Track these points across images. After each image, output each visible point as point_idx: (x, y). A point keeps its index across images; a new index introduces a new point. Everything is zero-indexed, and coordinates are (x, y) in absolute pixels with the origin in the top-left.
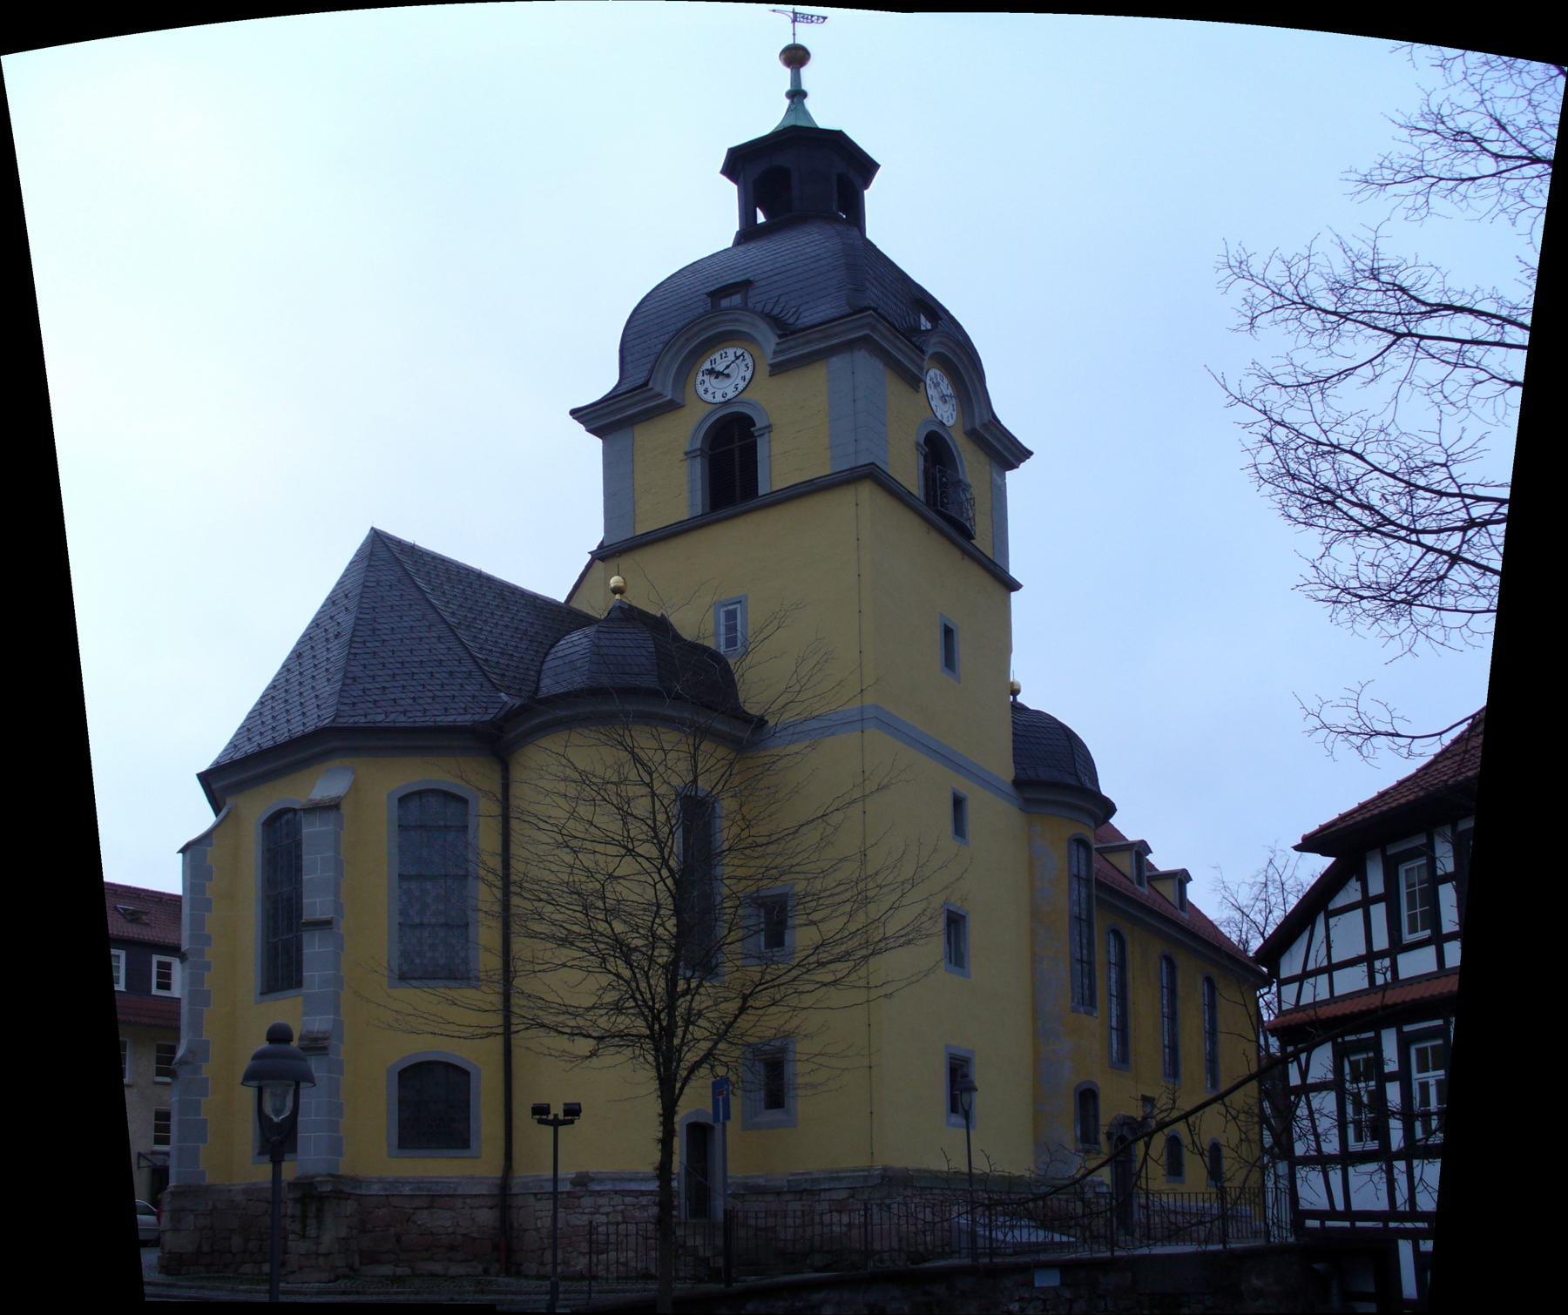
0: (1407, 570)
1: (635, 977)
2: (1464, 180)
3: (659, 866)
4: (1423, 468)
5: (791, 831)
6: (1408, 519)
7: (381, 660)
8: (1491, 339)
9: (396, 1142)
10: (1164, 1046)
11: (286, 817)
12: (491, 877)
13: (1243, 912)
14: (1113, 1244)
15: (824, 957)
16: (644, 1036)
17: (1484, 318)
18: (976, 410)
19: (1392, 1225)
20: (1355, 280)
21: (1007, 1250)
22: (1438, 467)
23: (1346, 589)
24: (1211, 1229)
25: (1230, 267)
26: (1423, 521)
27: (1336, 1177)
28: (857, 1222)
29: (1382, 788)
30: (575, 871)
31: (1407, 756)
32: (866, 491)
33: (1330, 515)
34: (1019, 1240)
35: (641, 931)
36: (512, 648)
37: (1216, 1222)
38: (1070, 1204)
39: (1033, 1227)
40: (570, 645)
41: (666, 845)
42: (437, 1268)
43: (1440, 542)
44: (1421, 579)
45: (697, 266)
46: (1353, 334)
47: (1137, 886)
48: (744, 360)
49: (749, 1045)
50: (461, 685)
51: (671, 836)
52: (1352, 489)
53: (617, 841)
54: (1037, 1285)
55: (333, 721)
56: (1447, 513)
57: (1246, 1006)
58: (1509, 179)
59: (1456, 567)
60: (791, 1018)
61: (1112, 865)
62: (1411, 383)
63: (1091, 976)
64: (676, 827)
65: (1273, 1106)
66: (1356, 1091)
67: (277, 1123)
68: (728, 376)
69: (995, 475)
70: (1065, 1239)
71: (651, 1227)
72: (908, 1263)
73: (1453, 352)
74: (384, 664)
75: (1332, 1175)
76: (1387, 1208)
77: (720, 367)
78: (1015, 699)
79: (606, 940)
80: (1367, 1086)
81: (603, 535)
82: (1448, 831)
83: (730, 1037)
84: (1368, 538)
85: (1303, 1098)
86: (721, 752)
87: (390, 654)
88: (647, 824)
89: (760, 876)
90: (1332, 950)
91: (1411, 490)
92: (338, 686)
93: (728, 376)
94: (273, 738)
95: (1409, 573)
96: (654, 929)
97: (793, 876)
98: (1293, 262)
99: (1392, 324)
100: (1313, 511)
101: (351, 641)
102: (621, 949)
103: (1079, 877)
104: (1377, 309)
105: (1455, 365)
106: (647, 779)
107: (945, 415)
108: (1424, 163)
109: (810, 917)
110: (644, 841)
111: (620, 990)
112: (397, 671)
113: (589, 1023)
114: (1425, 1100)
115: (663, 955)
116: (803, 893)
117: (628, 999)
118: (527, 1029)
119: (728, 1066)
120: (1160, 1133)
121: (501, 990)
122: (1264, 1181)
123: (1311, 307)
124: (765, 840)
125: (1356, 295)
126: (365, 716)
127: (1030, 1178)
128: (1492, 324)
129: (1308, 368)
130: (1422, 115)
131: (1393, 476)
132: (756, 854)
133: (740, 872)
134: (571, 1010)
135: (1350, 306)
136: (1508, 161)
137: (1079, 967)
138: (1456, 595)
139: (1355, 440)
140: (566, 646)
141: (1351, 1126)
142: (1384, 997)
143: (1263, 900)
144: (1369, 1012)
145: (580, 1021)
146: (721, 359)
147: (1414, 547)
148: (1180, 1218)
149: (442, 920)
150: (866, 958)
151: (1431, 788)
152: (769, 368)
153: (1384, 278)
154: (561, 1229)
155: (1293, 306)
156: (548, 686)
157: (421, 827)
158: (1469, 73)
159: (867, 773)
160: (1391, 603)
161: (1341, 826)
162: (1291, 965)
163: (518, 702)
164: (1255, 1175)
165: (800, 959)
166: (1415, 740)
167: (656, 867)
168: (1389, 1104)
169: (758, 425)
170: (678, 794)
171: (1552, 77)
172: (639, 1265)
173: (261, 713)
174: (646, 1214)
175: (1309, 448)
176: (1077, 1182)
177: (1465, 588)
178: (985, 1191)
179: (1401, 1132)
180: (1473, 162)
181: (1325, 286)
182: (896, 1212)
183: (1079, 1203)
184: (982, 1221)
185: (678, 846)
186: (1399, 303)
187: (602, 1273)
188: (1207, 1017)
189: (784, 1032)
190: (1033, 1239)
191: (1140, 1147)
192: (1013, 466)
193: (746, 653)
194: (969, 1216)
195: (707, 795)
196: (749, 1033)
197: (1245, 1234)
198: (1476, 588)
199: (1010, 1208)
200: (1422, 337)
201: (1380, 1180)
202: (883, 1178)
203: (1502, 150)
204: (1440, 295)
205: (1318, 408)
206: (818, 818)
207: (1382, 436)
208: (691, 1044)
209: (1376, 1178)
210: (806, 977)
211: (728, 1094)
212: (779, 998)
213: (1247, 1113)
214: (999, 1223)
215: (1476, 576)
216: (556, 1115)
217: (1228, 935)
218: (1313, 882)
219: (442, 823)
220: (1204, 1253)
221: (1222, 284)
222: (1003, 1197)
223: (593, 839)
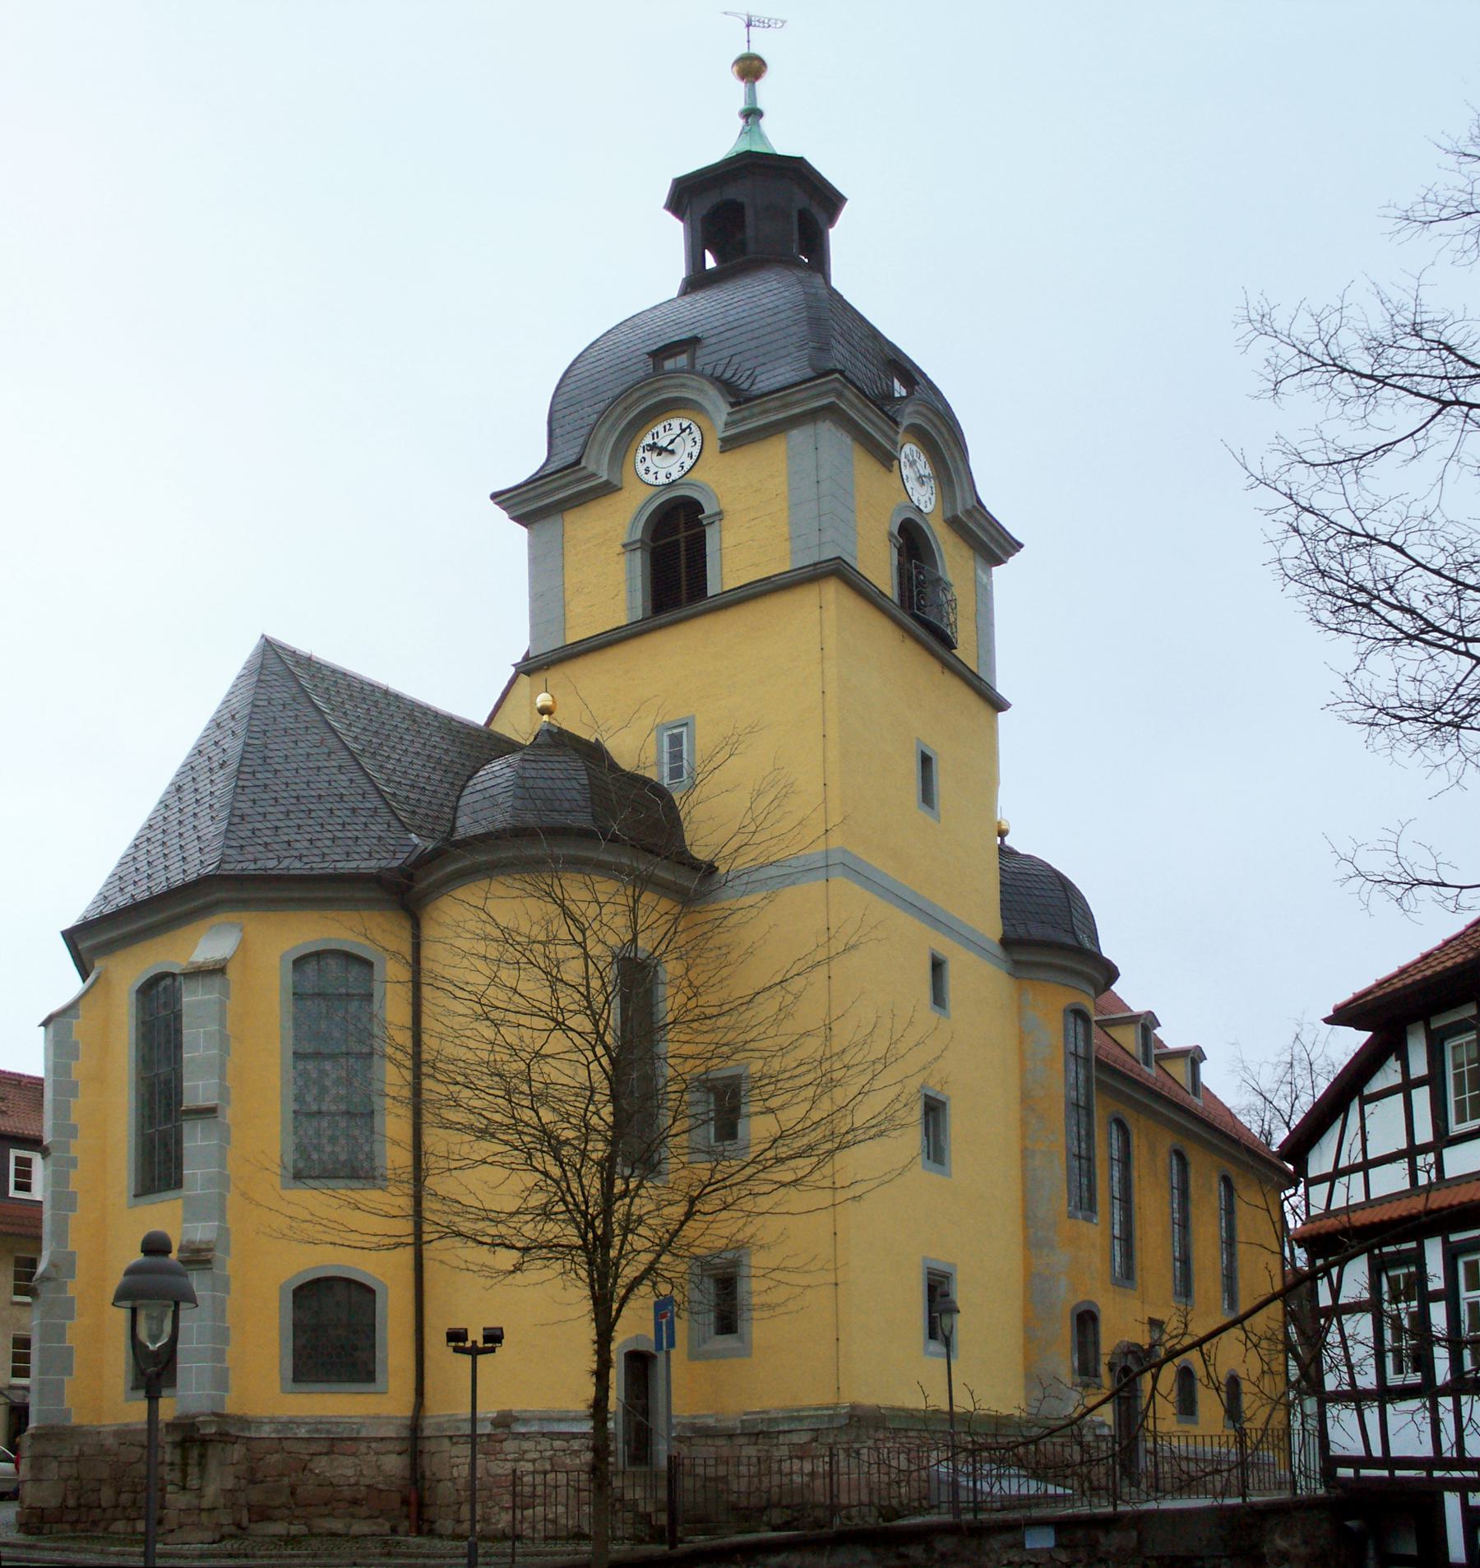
0: (1454, 686)
1: (566, 1176)
7: (274, 795)
9: (290, 1373)
11: (163, 984)
12: (399, 1056)
14: (1115, 1497)
15: (783, 1151)
16: (575, 1247)
18: (958, 494)
19: (1437, 1474)
24: (1228, 1480)
26: (1472, 627)
27: (1372, 1416)
28: (821, 1470)
29: (1426, 949)
30: (497, 1048)
32: (832, 592)
35: (572, 1120)
37: (1235, 1471)
39: (1024, 1476)
40: (491, 776)
41: (600, 1017)
42: (338, 1526)
44: (1470, 697)
46: (1392, 402)
47: (1143, 1066)
48: (690, 433)
49: (696, 1258)
50: (365, 824)
52: (1391, 589)
55: (218, 867)
57: (1268, 1211)
60: (745, 1225)
63: (1091, 1175)
65: (1301, 1332)
67: (153, 1352)
68: (672, 452)
69: (979, 572)
70: (1060, 1490)
71: (584, 1477)
72: (880, 1520)
74: (276, 799)
75: (1367, 1413)
79: (533, 1131)
80: (1409, 1307)
81: (528, 643)
85: (1335, 1321)
86: (665, 905)
87: (284, 787)
89: (709, 1055)
92: (223, 826)
93: (672, 452)
94: (149, 888)
95: (1456, 690)
98: (1323, 316)
101: (239, 772)
102: (549, 1142)
103: (1076, 1055)
104: (1420, 372)
106: (579, 938)
107: (922, 500)
109: (768, 1104)
110: (576, 1012)
112: (292, 808)
115: (598, 1149)
118: (440, 1238)
119: (672, 1283)
121: (411, 1192)
122: (1289, 1420)
123: (1344, 370)
124: (715, 1011)
126: (255, 861)
129: (1341, 443)
131: (1438, 573)
132: (705, 1028)
133: (686, 1050)
135: (1388, 367)
137: (1077, 1164)
140: (487, 777)
141: (1390, 1354)
144: (1411, 1218)
145: (503, 1229)
146: (664, 432)
147: (1462, 658)
148: (1192, 1466)
149: (343, 1107)
150: (831, 1153)
152: (719, 443)
153: (1427, 334)
154: (481, 1479)
155: (1323, 369)
156: (466, 826)
157: (319, 995)
159: (832, 931)
162: (1320, 1161)
163: (430, 845)
164: (1280, 1415)
169: (708, 512)
170: (614, 956)
172: (570, 1523)
173: (134, 859)
174: (578, 1461)
175: (1341, 539)
176: (1074, 1422)
178: (968, 1433)
181: (1360, 344)
182: (866, 1458)
183: (1077, 1448)
184: (964, 1469)
185: (615, 1019)
187: (528, 1532)
190: (1024, 1491)
191: (1146, 1380)
192: (999, 561)
193: (694, 786)
195: (648, 957)
196: (696, 1243)
200: (1472, 406)
201: (1424, 1420)
202: (851, 1417)
205: (1352, 491)
207: (1425, 525)
208: (630, 1257)
209: (1418, 1418)
210: (762, 1175)
213: (1269, 1339)
214: (985, 1472)
216: (474, 1342)
217: (1248, 1126)
218: (1346, 1061)
219: (343, 991)
220: (1221, 1508)
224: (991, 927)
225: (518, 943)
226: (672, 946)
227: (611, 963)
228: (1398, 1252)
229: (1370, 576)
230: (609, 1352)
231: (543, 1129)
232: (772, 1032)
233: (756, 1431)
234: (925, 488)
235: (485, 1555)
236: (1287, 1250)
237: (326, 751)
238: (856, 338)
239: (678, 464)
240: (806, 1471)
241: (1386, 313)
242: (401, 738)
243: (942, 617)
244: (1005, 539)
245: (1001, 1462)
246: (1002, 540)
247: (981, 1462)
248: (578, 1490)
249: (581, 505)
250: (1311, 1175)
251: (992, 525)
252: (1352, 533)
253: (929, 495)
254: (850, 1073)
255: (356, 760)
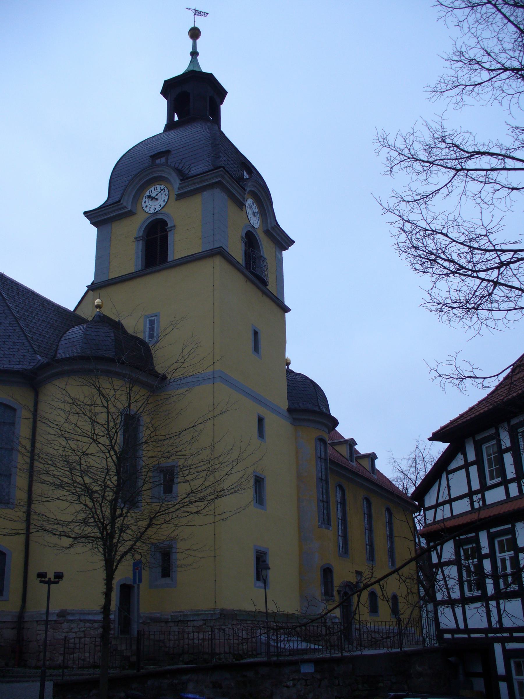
0: (473, 292)
2: (476, 85)
3: (109, 449)
4: (476, 238)
5: (177, 434)
6: (471, 265)
8: (499, 167)
10: (366, 545)
12: (23, 450)
13: (404, 474)
14: (342, 650)
15: (192, 499)
17: (495, 156)
19: (490, 635)
20: (435, 143)
21: (286, 653)
22: (483, 237)
23: (445, 304)
24: (393, 641)
25: (379, 141)
26: (479, 265)
27: (459, 611)
28: (207, 638)
29: (471, 406)
30: (66, 449)
31: (482, 388)
32: (218, 261)
33: (434, 267)
34: (292, 648)
36: (45, 333)
37: (396, 637)
38: (319, 628)
39: (300, 641)
41: (113, 438)
43: (488, 275)
44: (481, 296)
45: (144, 143)
46: (436, 172)
47: (350, 462)
49: (152, 544)
50: (18, 349)
51: (116, 434)
52: (443, 252)
53: (89, 435)
54: (302, 672)
56: (490, 260)
57: (408, 522)
58: (496, 81)
59: (497, 288)
60: (174, 530)
61: (338, 452)
62: (466, 194)
63: (328, 509)
64: (119, 429)
65: (425, 575)
66: (468, 564)
68: (157, 199)
69: (277, 253)
70: (316, 647)
71: (98, 640)
72: (234, 660)
73: (483, 176)
75: (457, 610)
76: (487, 627)
77: (153, 195)
78: (288, 367)
79: (80, 486)
80: (473, 562)
82: (506, 425)
83: (143, 539)
84: (453, 277)
85: (440, 570)
86: (143, 392)
88: (104, 427)
89: (160, 456)
90: (451, 491)
91: (472, 250)
93: (157, 199)
95: (474, 293)
96: (106, 482)
97: (178, 457)
98: (407, 137)
99: (454, 165)
100: (426, 265)
102: (88, 491)
103: (321, 458)
104: (446, 158)
105: (485, 183)
106: (106, 404)
107: (255, 222)
108: (458, 78)
109: (186, 478)
110: (102, 436)
111: (86, 513)
113: (69, 530)
114: (504, 568)
115: (110, 495)
116: (182, 466)
117: (91, 518)
118: (37, 531)
119: (141, 555)
120: (366, 590)
122: (421, 614)
123: (417, 160)
124: (163, 438)
125: (436, 151)
127: (298, 615)
128: (499, 159)
129: (419, 191)
130: (454, 53)
131: (462, 244)
132: (158, 445)
133: (150, 454)
134: (60, 522)
135: (434, 157)
136: (494, 72)
138: (499, 302)
139: (443, 227)
141: (466, 583)
142: (479, 514)
143: (414, 467)
144: (472, 523)
145: (65, 528)
146: (155, 190)
147: (476, 279)
148: (377, 635)
150: (213, 500)
151: (495, 404)
152: (175, 196)
153: (448, 141)
155: (409, 160)
156: (61, 354)
158: (471, 28)
159: (216, 405)
160: (467, 309)
161: (451, 427)
162: (430, 500)
163: (45, 361)
164: (416, 611)
165: (180, 500)
166: (485, 379)
167: (108, 450)
168: (485, 571)
169: (169, 225)
171: (505, 24)
175: (422, 233)
176: (322, 617)
177: (502, 298)
178: (275, 622)
179: (492, 586)
180: (479, 75)
181: (422, 148)
182: (228, 633)
183: (324, 628)
184: (273, 638)
186: (456, 153)
188: (388, 529)
189: (171, 537)
190: (300, 647)
191: (355, 598)
192: (286, 249)
193: (157, 342)
194: (266, 635)
196: (152, 537)
197: (411, 643)
198: (508, 297)
199: (288, 631)
200: (468, 170)
201: (483, 611)
202: (221, 614)
203: (490, 67)
204: (474, 147)
205: (424, 211)
206: (191, 427)
207: (455, 224)
209: (480, 611)
210: (182, 509)
211: (141, 570)
212: (169, 520)
213: (410, 578)
214: (282, 639)
215: (507, 292)
217: (397, 486)
218: (439, 457)
220: (391, 653)
221: (376, 151)
222: (284, 625)
223: (76, 433)
224: (283, 404)
225: (79, 405)
226: (145, 409)
227: (119, 416)
228: (467, 538)
229: (434, 248)
230: (111, 584)
231: (85, 485)
232: (188, 448)
233: (177, 620)
234: (256, 217)
235: (51, 675)
236: (417, 539)
237: (5, 316)
238: (229, 152)
239: (159, 204)
240: (200, 638)
241: (430, 133)
242: (37, 314)
243: (262, 272)
244: (288, 239)
245: (289, 634)
246: (286, 240)
247: (280, 634)
248: (96, 646)
249: (119, 220)
250: (426, 506)
251: (282, 233)
252: (426, 230)
253: (257, 220)
254: (223, 465)
255: (17, 321)
